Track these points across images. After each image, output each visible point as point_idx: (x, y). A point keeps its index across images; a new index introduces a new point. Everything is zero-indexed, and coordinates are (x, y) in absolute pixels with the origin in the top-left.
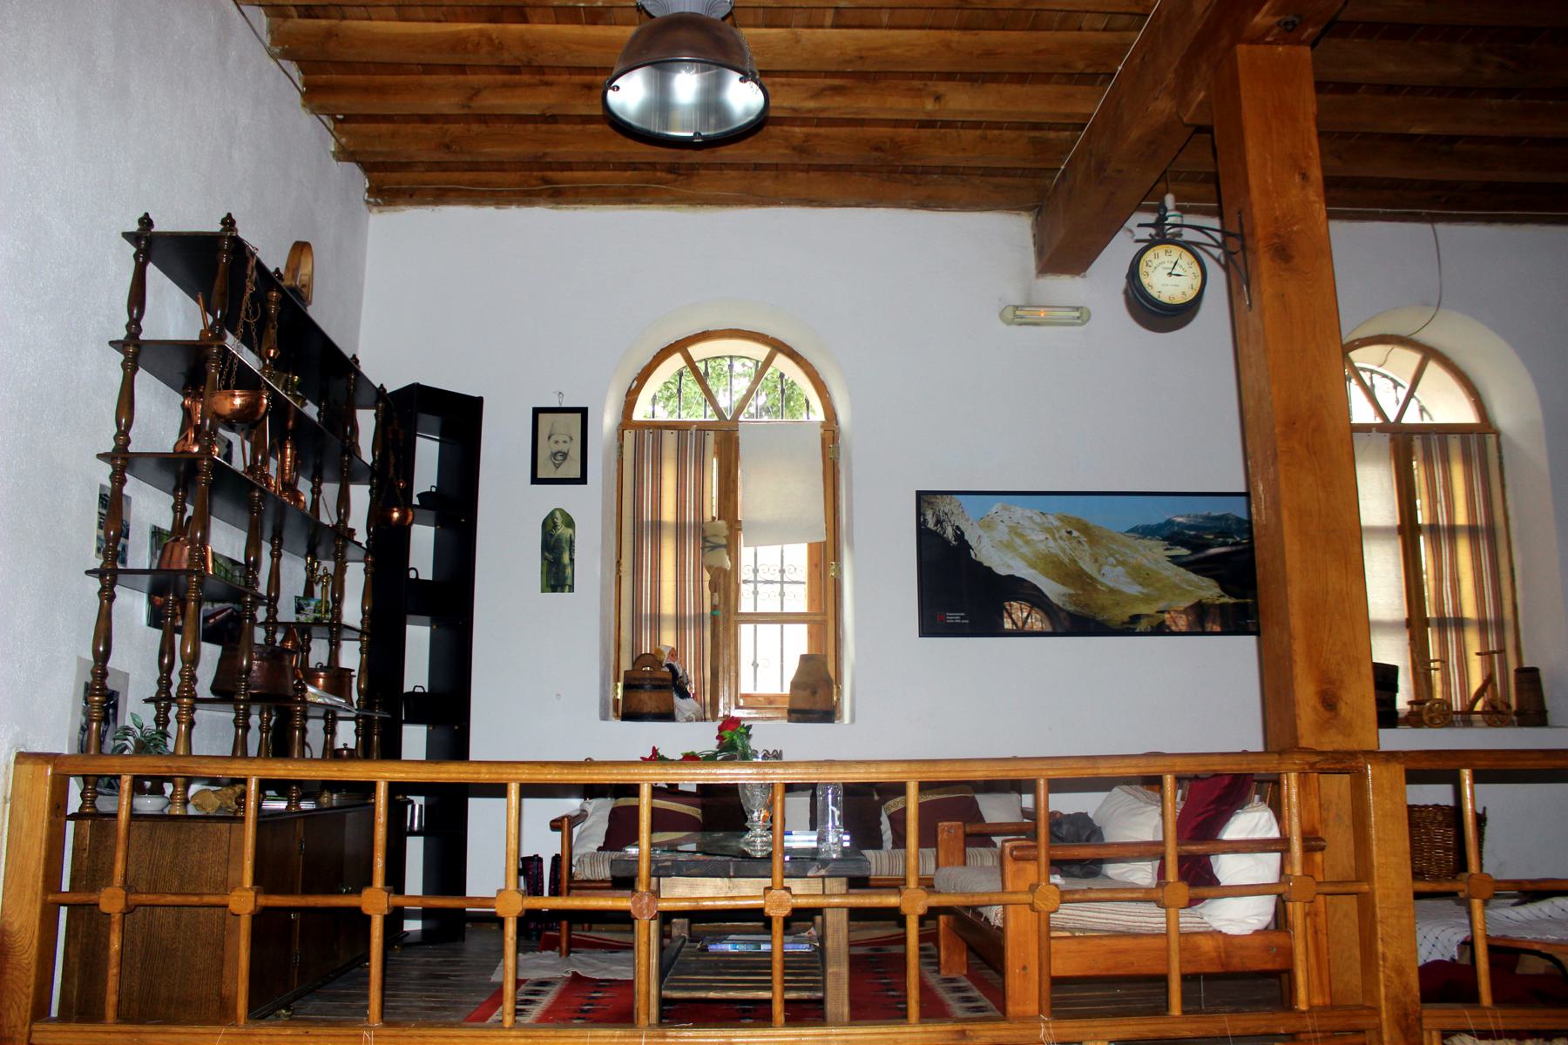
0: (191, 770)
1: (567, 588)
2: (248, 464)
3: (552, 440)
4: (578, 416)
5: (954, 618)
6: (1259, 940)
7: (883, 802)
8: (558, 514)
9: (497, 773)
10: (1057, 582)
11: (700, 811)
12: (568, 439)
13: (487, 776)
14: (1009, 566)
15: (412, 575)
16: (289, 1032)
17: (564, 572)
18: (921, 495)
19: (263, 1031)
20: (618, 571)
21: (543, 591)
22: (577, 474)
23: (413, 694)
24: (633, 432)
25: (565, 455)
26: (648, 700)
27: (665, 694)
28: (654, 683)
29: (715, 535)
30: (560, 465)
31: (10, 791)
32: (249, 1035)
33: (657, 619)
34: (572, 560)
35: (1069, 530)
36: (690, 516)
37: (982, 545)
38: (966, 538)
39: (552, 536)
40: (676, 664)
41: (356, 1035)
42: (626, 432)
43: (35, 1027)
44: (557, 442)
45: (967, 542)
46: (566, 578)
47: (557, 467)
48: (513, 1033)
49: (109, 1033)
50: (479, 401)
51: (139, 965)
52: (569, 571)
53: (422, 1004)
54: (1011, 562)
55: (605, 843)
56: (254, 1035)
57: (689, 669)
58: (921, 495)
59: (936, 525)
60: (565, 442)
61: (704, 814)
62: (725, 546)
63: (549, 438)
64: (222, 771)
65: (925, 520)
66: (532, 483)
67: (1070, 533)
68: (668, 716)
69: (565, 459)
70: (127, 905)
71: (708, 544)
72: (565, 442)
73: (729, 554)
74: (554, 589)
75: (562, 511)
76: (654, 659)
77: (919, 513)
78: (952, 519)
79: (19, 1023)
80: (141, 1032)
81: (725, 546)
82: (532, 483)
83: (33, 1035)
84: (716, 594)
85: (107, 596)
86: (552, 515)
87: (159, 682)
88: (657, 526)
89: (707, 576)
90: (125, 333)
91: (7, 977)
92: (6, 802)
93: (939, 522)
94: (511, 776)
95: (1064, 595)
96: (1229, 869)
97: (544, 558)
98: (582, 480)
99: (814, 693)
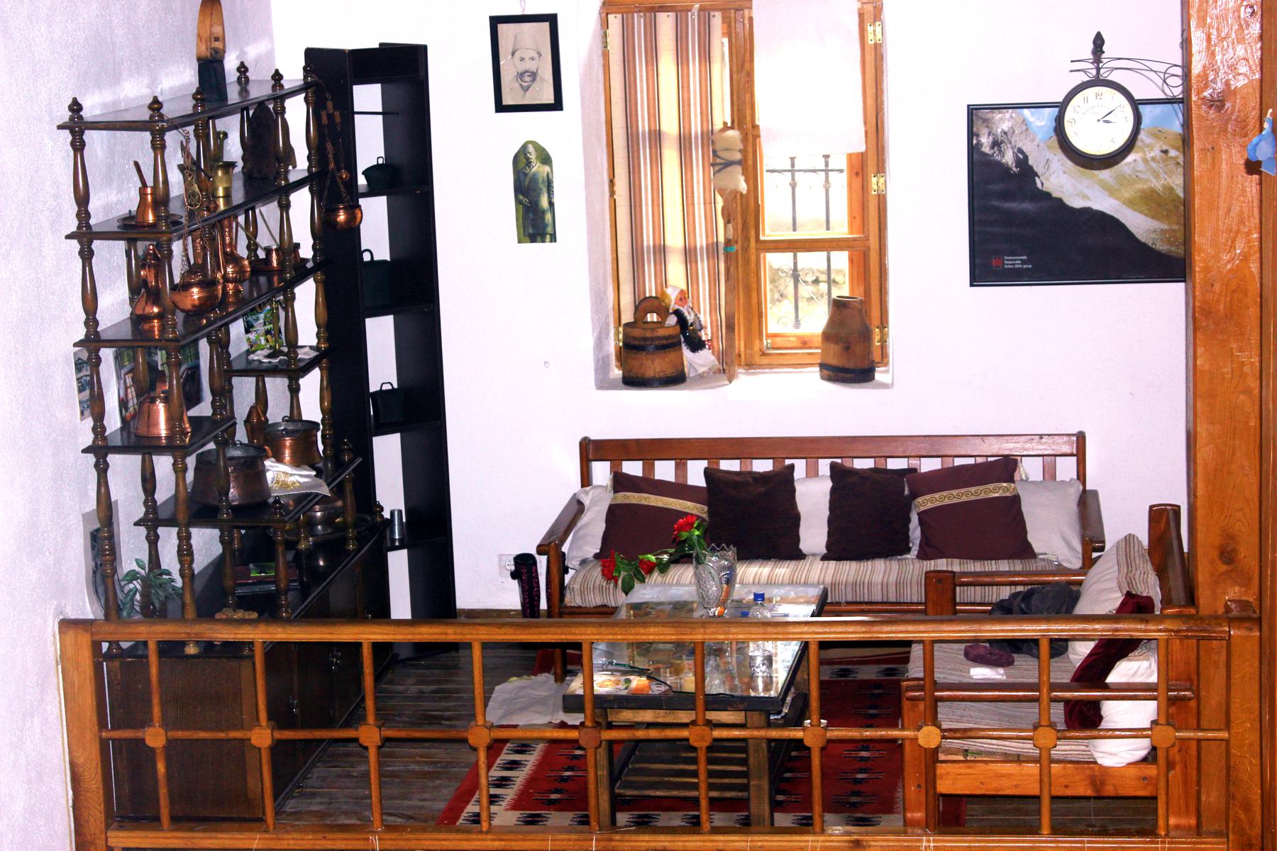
0: (207, 635)
1: (548, 237)
2: (192, 262)
3: (518, 55)
4: (546, 26)
5: (1014, 262)
6: (1133, 771)
7: (914, 495)
8: (531, 148)
9: (461, 634)
10: (1146, 215)
11: (706, 508)
12: (536, 55)
13: (453, 637)
14: (1085, 197)
15: (367, 257)
16: (310, 837)
17: (544, 219)
18: (973, 111)
19: (289, 837)
20: (612, 193)
21: (520, 241)
22: (549, 98)
23: (381, 392)
24: (619, 16)
25: (534, 75)
26: (655, 365)
27: (671, 356)
28: (657, 343)
29: (726, 150)
30: (528, 88)
31: (59, 653)
32: (279, 839)
33: (661, 251)
34: (551, 204)
35: (1165, 148)
36: (696, 127)
37: (1051, 171)
38: (1030, 162)
39: (526, 175)
40: (684, 310)
41: (364, 839)
42: (611, 17)
43: (109, 834)
44: (522, 59)
45: (1031, 168)
46: (545, 226)
47: (526, 89)
48: (489, 837)
49: (168, 838)
50: (424, 48)
51: (176, 775)
52: (548, 217)
53: (417, 768)
54: (1088, 192)
55: (601, 549)
56: (283, 839)
57: (705, 317)
58: (973, 111)
59: (992, 147)
60: (532, 59)
61: (710, 513)
62: (739, 163)
63: (513, 54)
64: (233, 636)
65: (979, 142)
66: (497, 111)
67: (1166, 152)
68: (676, 379)
69: (534, 80)
70: (168, 740)
71: (718, 161)
72: (532, 59)
73: (745, 173)
74: (533, 239)
75: (535, 144)
76: (657, 304)
77: (971, 134)
78: (1013, 140)
79: (97, 831)
80: (193, 838)
81: (739, 163)
82: (497, 111)
83: (109, 839)
84: (730, 226)
85: (102, 469)
86: (524, 149)
87: (86, 323)
88: (656, 137)
89: (720, 202)
90: (76, 223)
91: (82, 797)
92: (57, 665)
93: (996, 144)
94: (474, 637)
95: (1155, 231)
96: (1117, 713)
97: (518, 202)
98: (557, 105)
99: (847, 349)
